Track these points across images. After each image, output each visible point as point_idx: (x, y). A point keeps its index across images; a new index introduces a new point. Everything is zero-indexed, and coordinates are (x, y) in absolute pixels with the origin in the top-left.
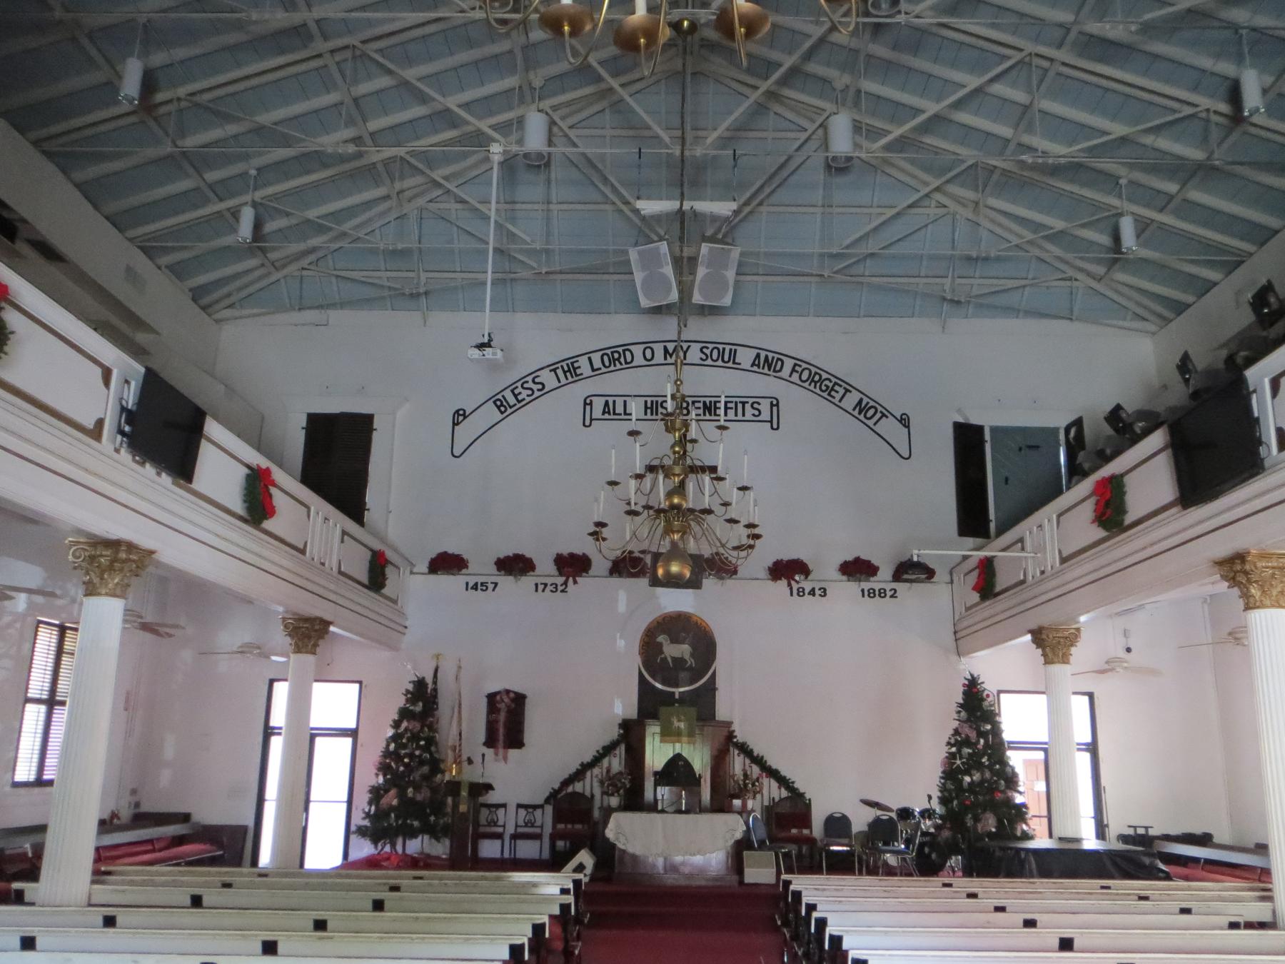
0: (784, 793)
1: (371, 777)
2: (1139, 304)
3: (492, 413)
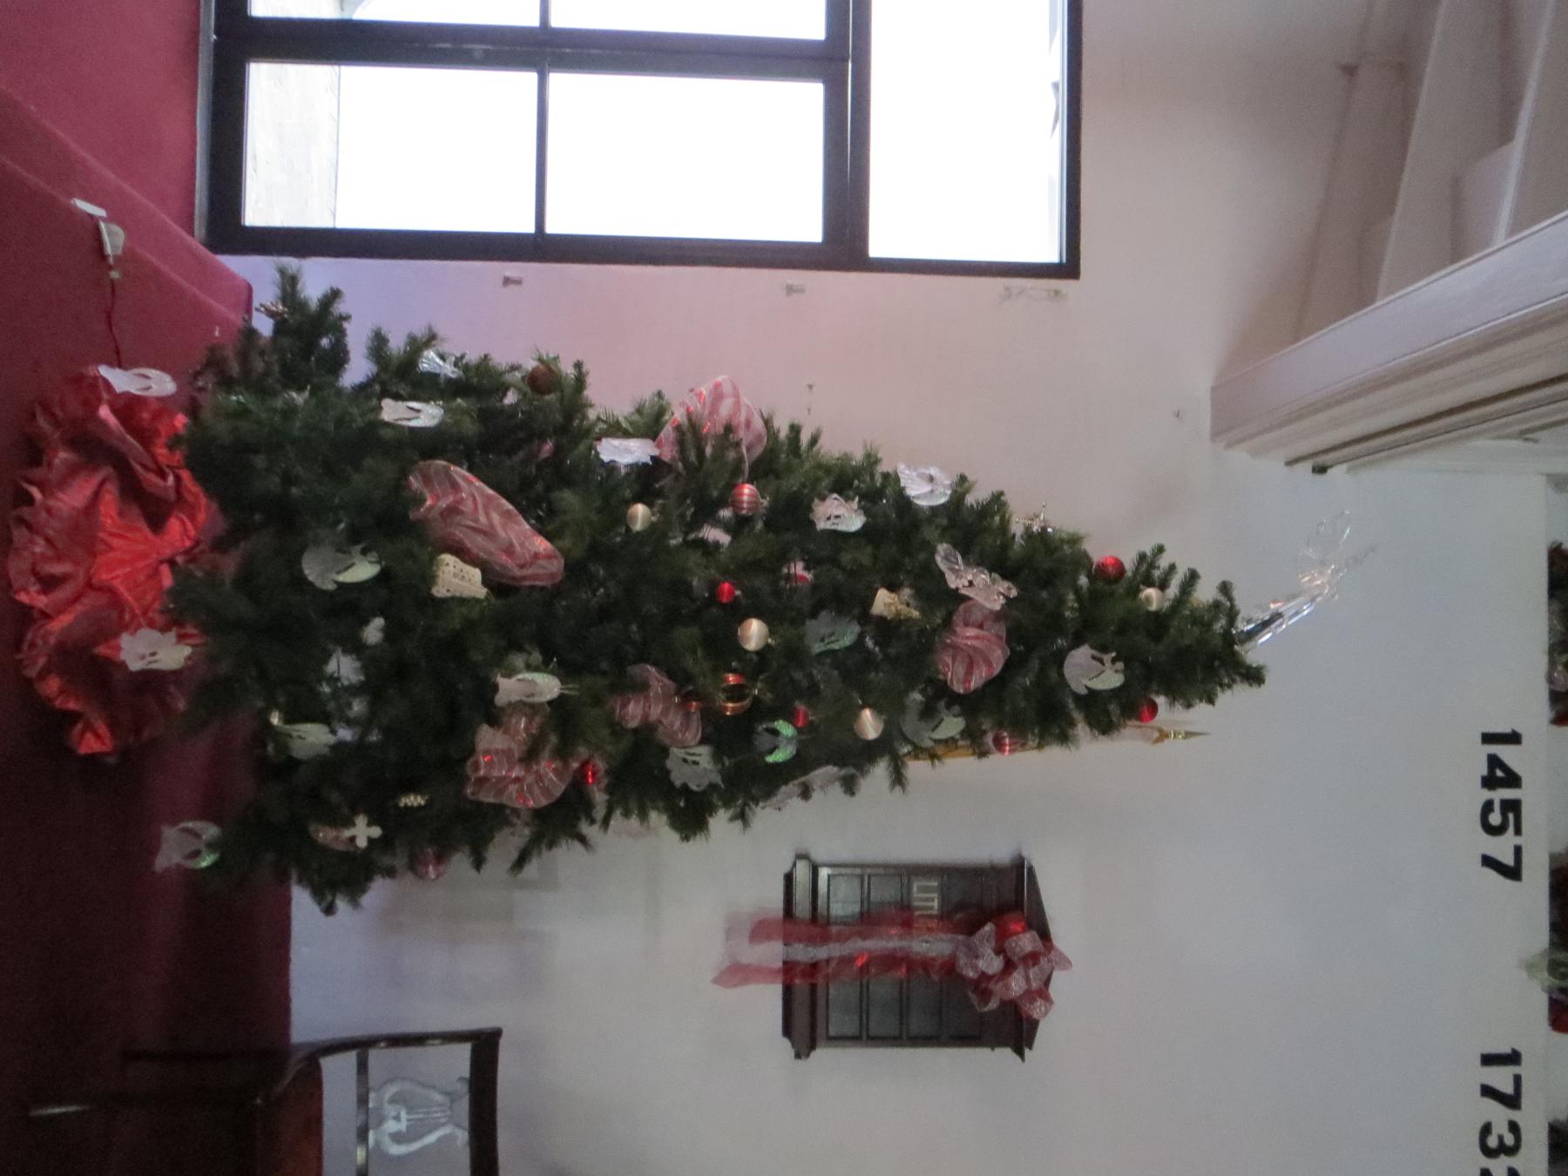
1: (638, 368)
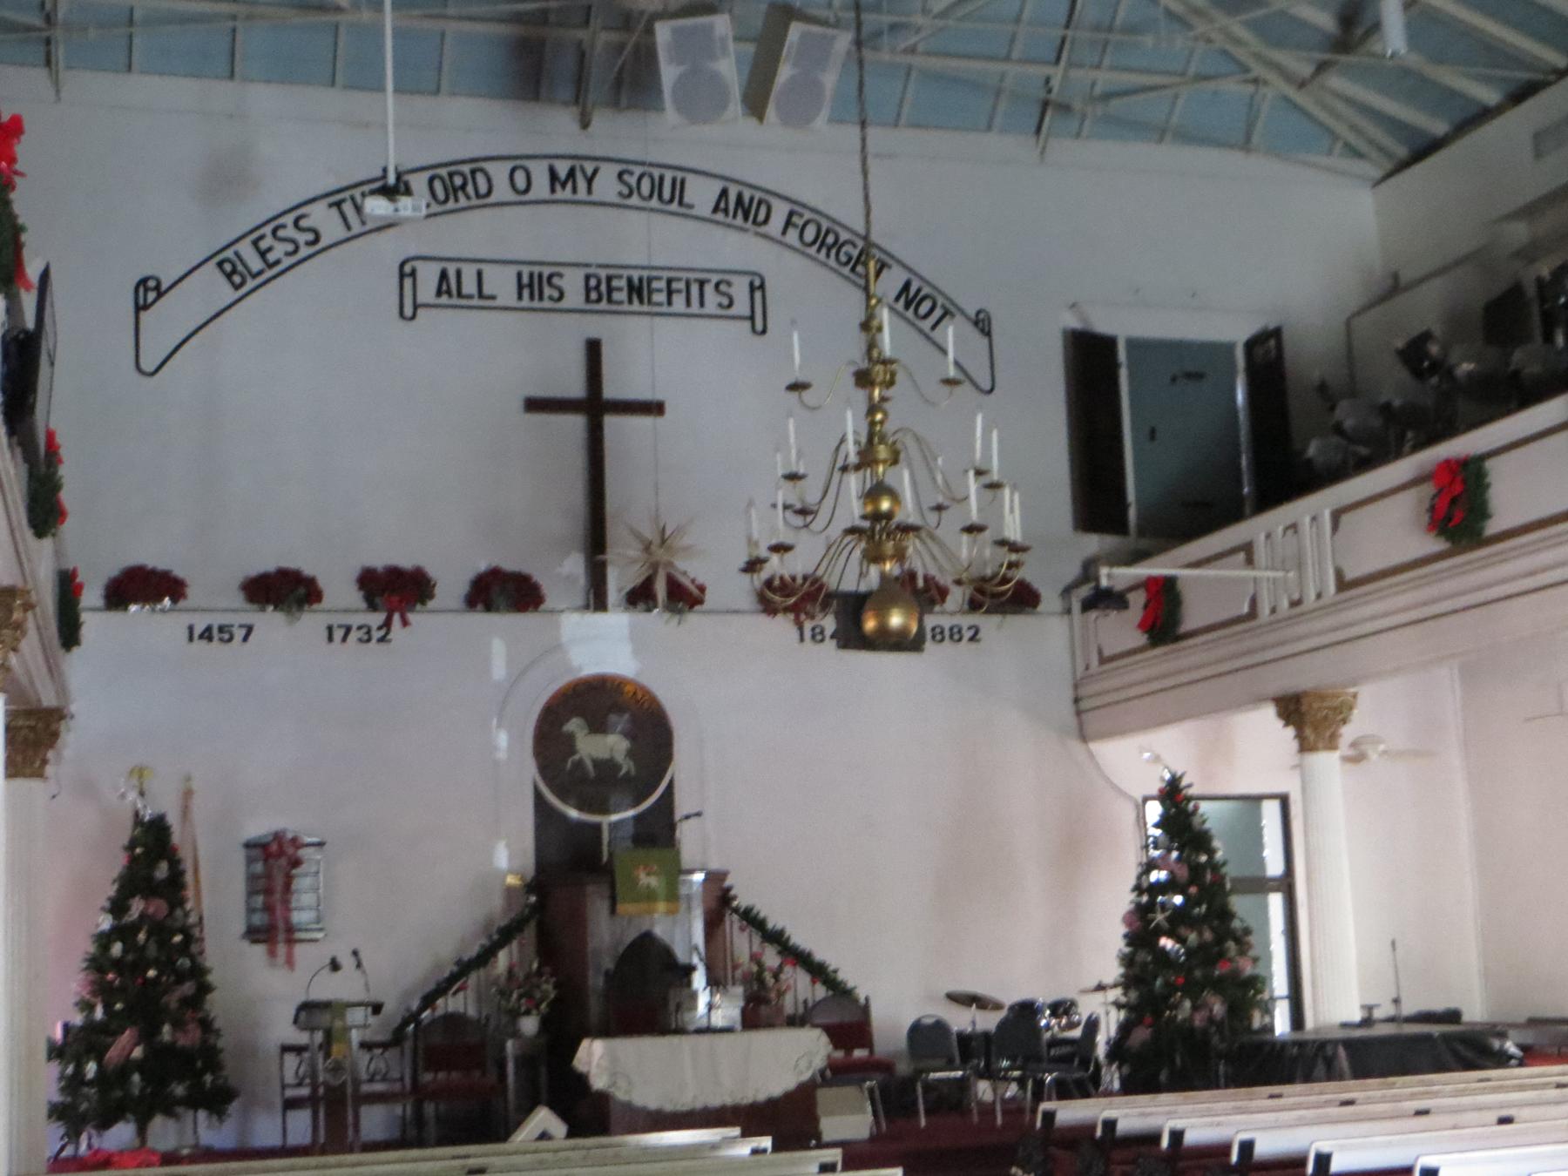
0: (821, 992)
2: (1353, 128)
3: (212, 288)
